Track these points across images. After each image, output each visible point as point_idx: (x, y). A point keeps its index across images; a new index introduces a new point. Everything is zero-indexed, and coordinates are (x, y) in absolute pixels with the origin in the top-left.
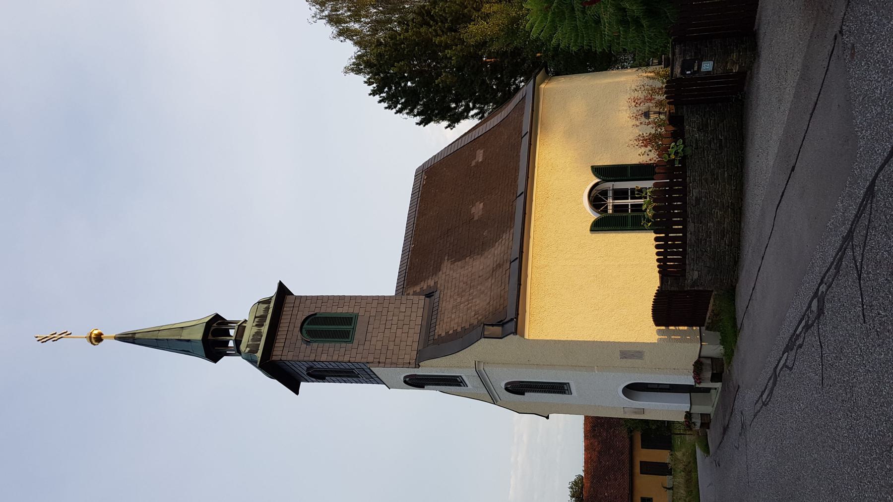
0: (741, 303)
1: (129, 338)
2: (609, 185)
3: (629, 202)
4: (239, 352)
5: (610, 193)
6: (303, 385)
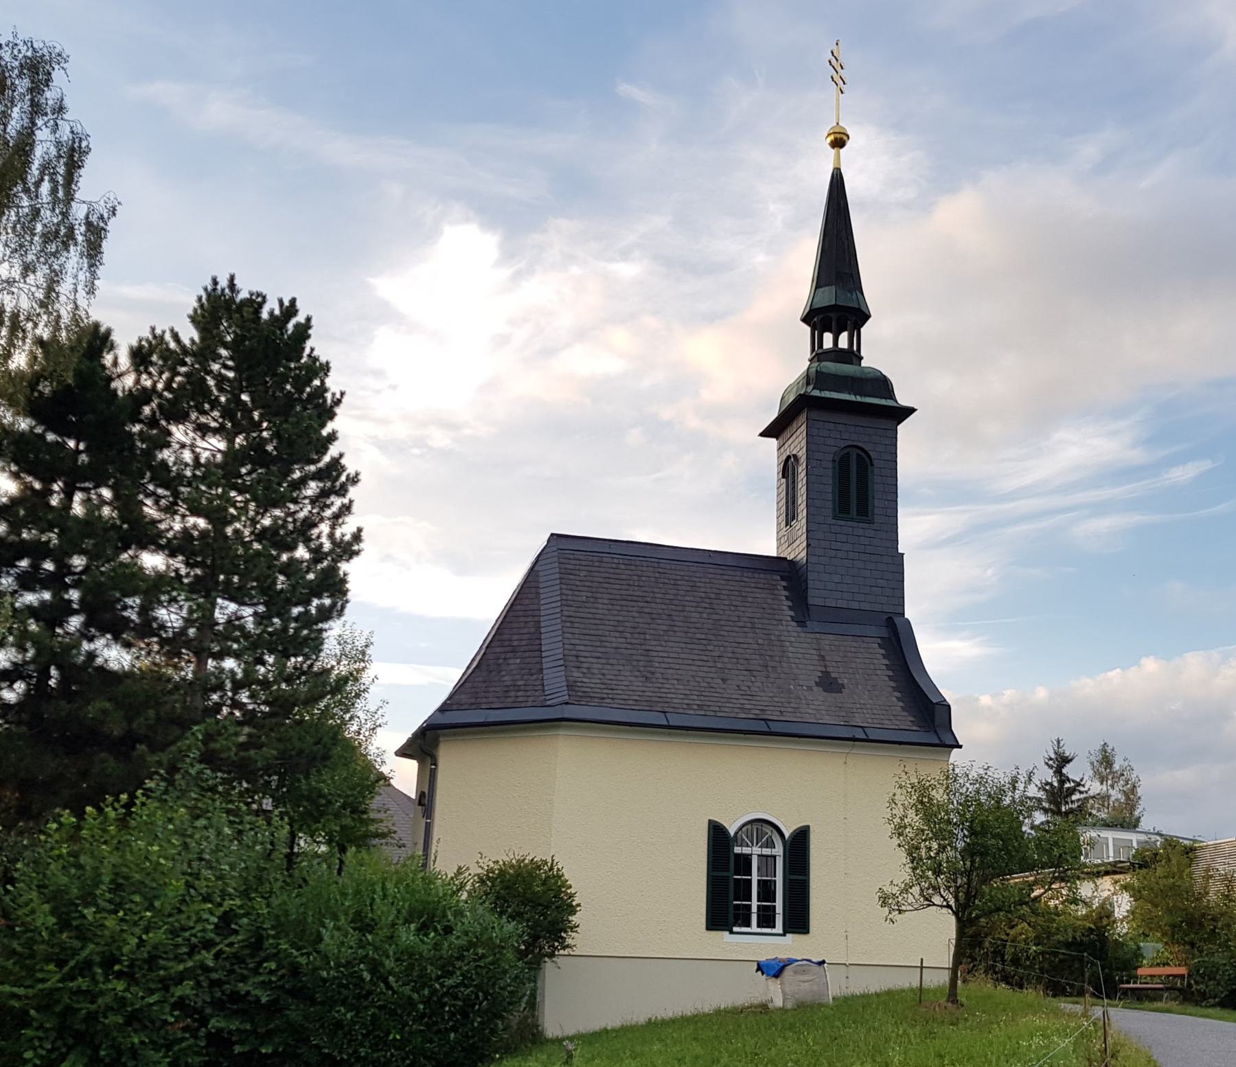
0: (874, 984)
1: (837, 184)
2: (778, 850)
3: (755, 904)
4: (819, 354)
5: (766, 851)
6: (772, 443)
